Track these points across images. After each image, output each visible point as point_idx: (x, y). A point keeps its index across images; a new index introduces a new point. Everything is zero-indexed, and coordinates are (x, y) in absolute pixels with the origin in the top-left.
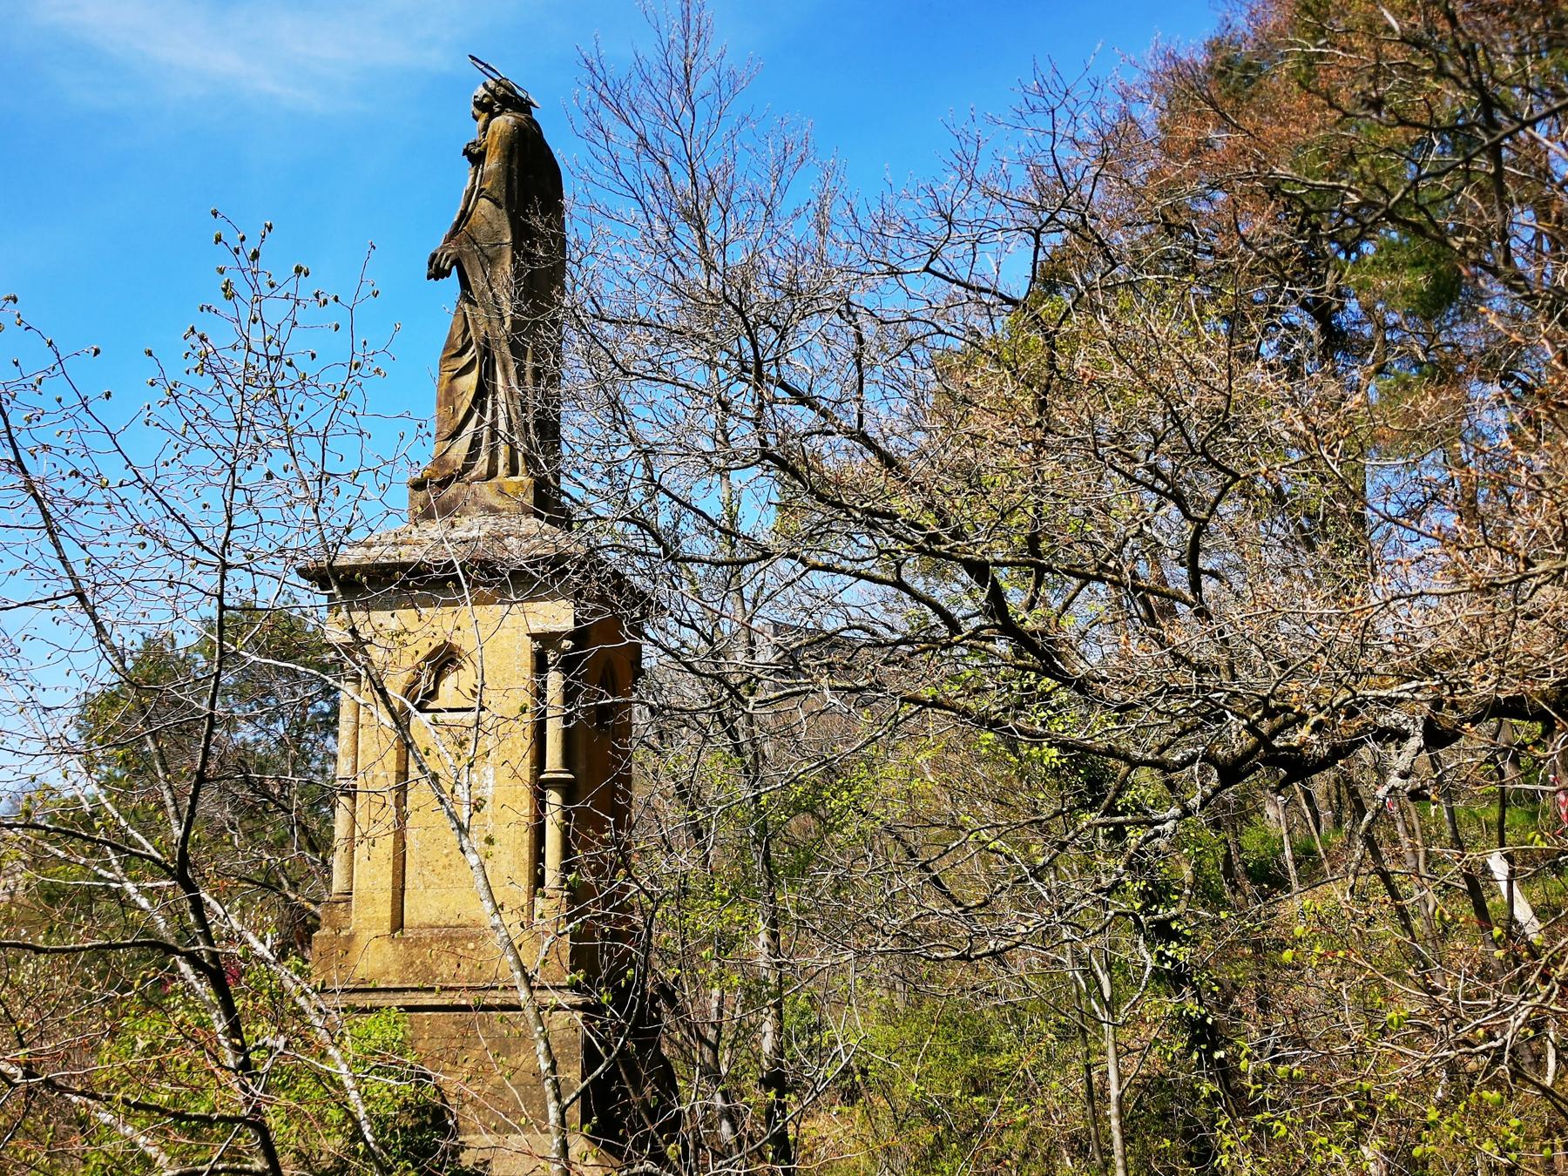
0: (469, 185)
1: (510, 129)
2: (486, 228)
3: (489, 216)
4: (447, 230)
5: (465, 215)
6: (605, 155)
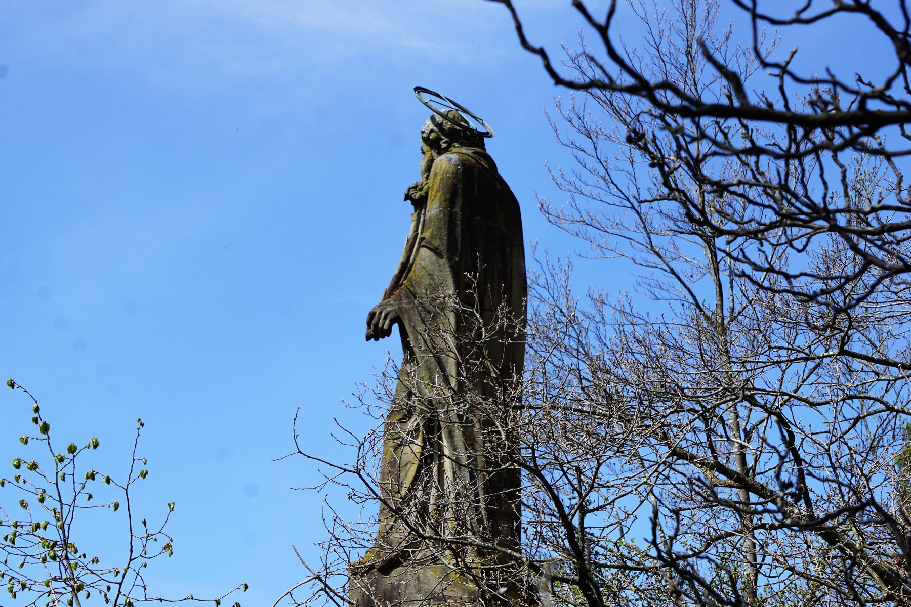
0: (410, 234)
1: (452, 169)
2: (427, 281)
3: (430, 267)
4: (387, 283)
5: (406, 267)
6: (592, 163)
